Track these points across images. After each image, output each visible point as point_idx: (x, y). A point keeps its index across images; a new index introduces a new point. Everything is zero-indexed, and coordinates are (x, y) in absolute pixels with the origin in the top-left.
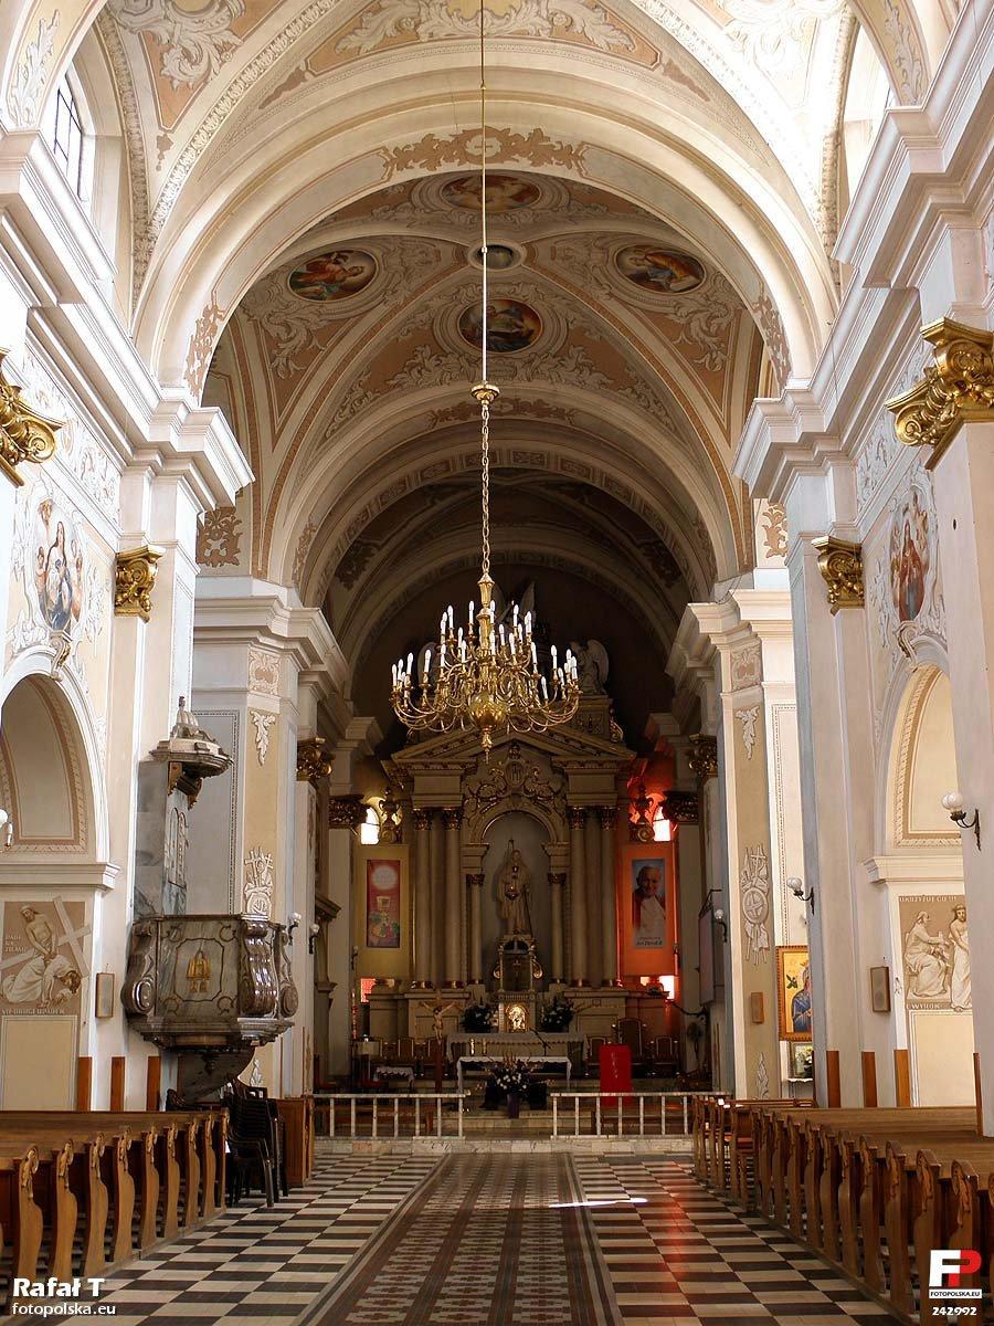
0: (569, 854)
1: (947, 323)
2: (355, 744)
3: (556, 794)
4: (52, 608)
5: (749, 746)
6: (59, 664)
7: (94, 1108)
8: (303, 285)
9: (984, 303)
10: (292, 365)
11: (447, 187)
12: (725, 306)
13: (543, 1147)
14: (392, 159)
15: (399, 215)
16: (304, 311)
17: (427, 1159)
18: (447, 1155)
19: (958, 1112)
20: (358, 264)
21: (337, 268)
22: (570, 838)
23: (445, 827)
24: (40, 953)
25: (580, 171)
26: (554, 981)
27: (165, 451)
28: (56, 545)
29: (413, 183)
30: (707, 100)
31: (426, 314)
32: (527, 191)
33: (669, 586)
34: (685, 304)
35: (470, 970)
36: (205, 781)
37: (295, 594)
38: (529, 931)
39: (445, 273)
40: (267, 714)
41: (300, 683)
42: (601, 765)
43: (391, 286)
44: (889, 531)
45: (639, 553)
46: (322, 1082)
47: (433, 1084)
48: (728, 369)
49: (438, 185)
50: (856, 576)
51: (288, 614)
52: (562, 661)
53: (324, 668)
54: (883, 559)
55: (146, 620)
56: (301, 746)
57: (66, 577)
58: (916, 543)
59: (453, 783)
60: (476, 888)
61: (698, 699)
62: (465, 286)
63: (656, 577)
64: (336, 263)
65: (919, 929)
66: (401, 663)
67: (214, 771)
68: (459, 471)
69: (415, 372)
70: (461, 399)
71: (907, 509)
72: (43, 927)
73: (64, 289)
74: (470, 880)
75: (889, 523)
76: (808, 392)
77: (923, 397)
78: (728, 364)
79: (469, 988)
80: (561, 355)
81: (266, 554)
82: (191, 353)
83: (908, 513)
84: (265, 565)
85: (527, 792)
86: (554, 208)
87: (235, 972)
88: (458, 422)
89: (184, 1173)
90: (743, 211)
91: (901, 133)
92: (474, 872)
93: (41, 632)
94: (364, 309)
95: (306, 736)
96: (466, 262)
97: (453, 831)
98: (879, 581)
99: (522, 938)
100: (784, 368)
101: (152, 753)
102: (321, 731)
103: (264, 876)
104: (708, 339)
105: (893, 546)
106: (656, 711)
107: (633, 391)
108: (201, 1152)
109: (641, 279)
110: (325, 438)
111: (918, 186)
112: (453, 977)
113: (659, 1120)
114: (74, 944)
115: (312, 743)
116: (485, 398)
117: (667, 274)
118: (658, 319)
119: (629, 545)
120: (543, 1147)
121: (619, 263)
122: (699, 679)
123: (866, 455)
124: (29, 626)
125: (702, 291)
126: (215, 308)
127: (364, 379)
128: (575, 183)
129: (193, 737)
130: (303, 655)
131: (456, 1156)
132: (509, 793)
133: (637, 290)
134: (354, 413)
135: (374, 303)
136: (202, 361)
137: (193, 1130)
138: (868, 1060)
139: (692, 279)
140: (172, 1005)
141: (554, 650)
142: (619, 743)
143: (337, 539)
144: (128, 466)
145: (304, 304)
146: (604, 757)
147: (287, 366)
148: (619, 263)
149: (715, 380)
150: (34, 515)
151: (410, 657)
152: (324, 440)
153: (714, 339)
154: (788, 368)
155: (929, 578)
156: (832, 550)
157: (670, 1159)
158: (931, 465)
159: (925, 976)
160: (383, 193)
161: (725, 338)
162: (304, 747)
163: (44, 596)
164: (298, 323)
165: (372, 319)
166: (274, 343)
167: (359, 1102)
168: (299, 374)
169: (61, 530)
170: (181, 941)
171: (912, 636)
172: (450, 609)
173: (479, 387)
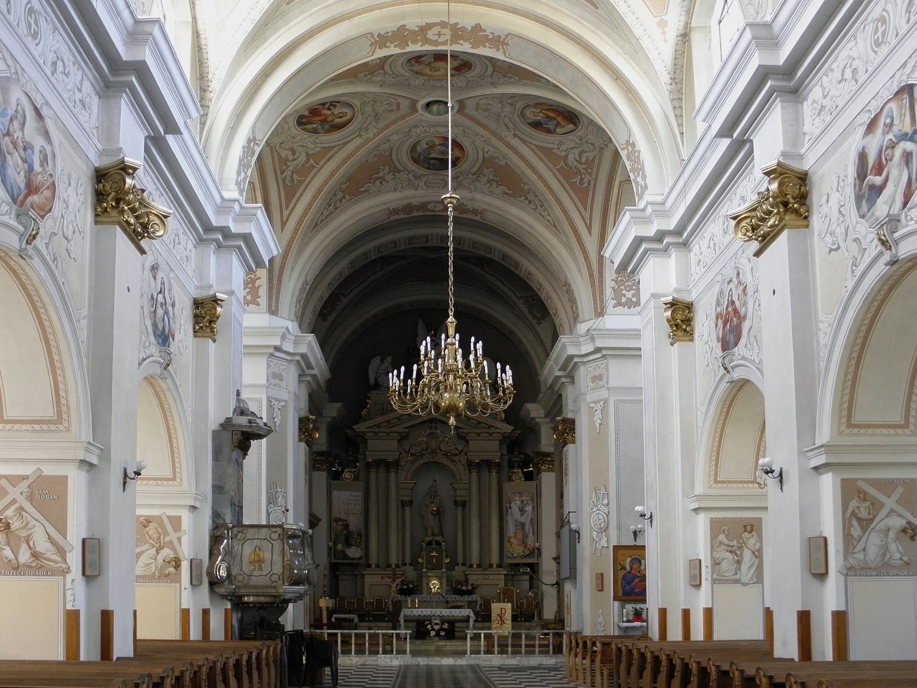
0: (469, 489)
1: (779, 164)
2: (330, 420)
3: (460, 452)
4: (159, 333)
5: (598, 425)
6: (165, 369)
7: (192, 638)
8: (305, 124)
9: (803, 151)
10: (295, 177)
11: (409, 61)
12: (593, 144)
13: (461, 662)
14: (376, 41)
15: (375, 79)
16: (307, 142)
17: (388, 669)
18: (400, 666)
19: (742, 643)
20: (344, 110)
21: (329, 112)
22: (470, 479)
23: (388, 472)
24: (153, 546)
25: (505, 53)
26: (458, 565)
27: (226, 232)
28: (160, 292)
29: (386, 58)
30: (597, 8)
31: (388, 144)
32: (463, 64)
33: (539, 324)
34: (564, 142)
35: (404, 559)
36: (254, 443)
37: (296, 324)
38: (442, 534)
39: (403, 117)
40: (279, 401)
41: (300, 381)
42: (490, 434)
43: (365, 126)
44: (716, 294)
45: (520, 303)
46: (457, 625)
47: (390, 624)
48: (591, 186)
49: (404, 58)
50: (688, 321)
51: (293, 338)
52: (504, 371)
53: (315, 372)
54: (709, 311)
55: (214, 341)
56: (301, 421)
57: (166, 313)
58: (737, 303)
59: (394, 444)
60: (407, 509)
61: (561, 395)
62: (416, 126)
63: (530, 317)
64: (329, 109)
65: (722, 537)
66: (395, 372)
67: (259, 437)
68: (403, 247)
69: (377, 182)
70: (408, 201)
71: (731, 281)
72: (155, 531)
73: (172, 127)
74: (403, 504)
75: (716, 289)
76: (663, 204)
77: (755, 210)
78: (592, 182)
79: (403, 568)
80: (479, 173)
81: (278, 298)
82: (239, 168)
83: (731, 284)
84: (277, 307)
85: (441, 450)
86: (482, 77)
87: (280, 559)
88: (406, 216)
89: (260, 677)
90: (617, 83)
91: (754, 38)
92: (407, 499)
93: (154, 349)
94: (345, 141)
95: (303, 414)
96: (416, 111)
97: (393, 475)
98: (705, 325)
99: (437, 538)
100: (642, 186)
101: (221, 425)
102: (311, 413)
103: (279, 500)
104: (579, 166)
105: (718, 304)
106: (529, 402)
107: (526, 199)
108: (268, 665)
109: (536, 125)
110: (316, 225)
111: (763, 74)
112: (393, 560)
113: (520, 646)
114: (175, 542)
115: (308, 419)
116: (451, 203)
117: (555, 122)
118: (547, 153)
119: (513, 297)
120: (461, 662)
121: (522, 114)
122: (563, 383)
123: (700, 246)
124: (147, 344)
125: (579, 134)
126: (254, 138)
127: (344, 186)
128: (499, 60)
129: (247, 415)
130: (303, 364)
131: (407, 667)
132: (429, 451)
133: (532, 132)
134: (336, 209)
135: (353, 136)
136: (246, 173)
137: (264, 652)
138: (686, 614)
139: (571, 126)
140: (240, 578)
141: (499, 365)
142: (502, 421)
143: (323, 291)
144: (201, 241)
145: (305, 136)
146: (493, 430)
147: (292, 177)
148: (522, 114)
149: (583, 194)
150: (148, 274)
151: (403, 369)
152: (316, 226)
153: (584, 166)
154: (646, 187)
155: (746, 326)
156: (674, 305)
157: (544, 669)
158: (758, 254)
159: (724, 565)
160: (366, 64)
161: (591, 166)
162: (303, 422)
163: (155, 325)
164: (301, 149)
165: (351, 147)
166: (284, 161)
167: (554, 634)
168: (300, 183)
169: (163, 283)
170: (245, 540)
171: (732, 361)
172: (428, 339)
173: (448, 195)
